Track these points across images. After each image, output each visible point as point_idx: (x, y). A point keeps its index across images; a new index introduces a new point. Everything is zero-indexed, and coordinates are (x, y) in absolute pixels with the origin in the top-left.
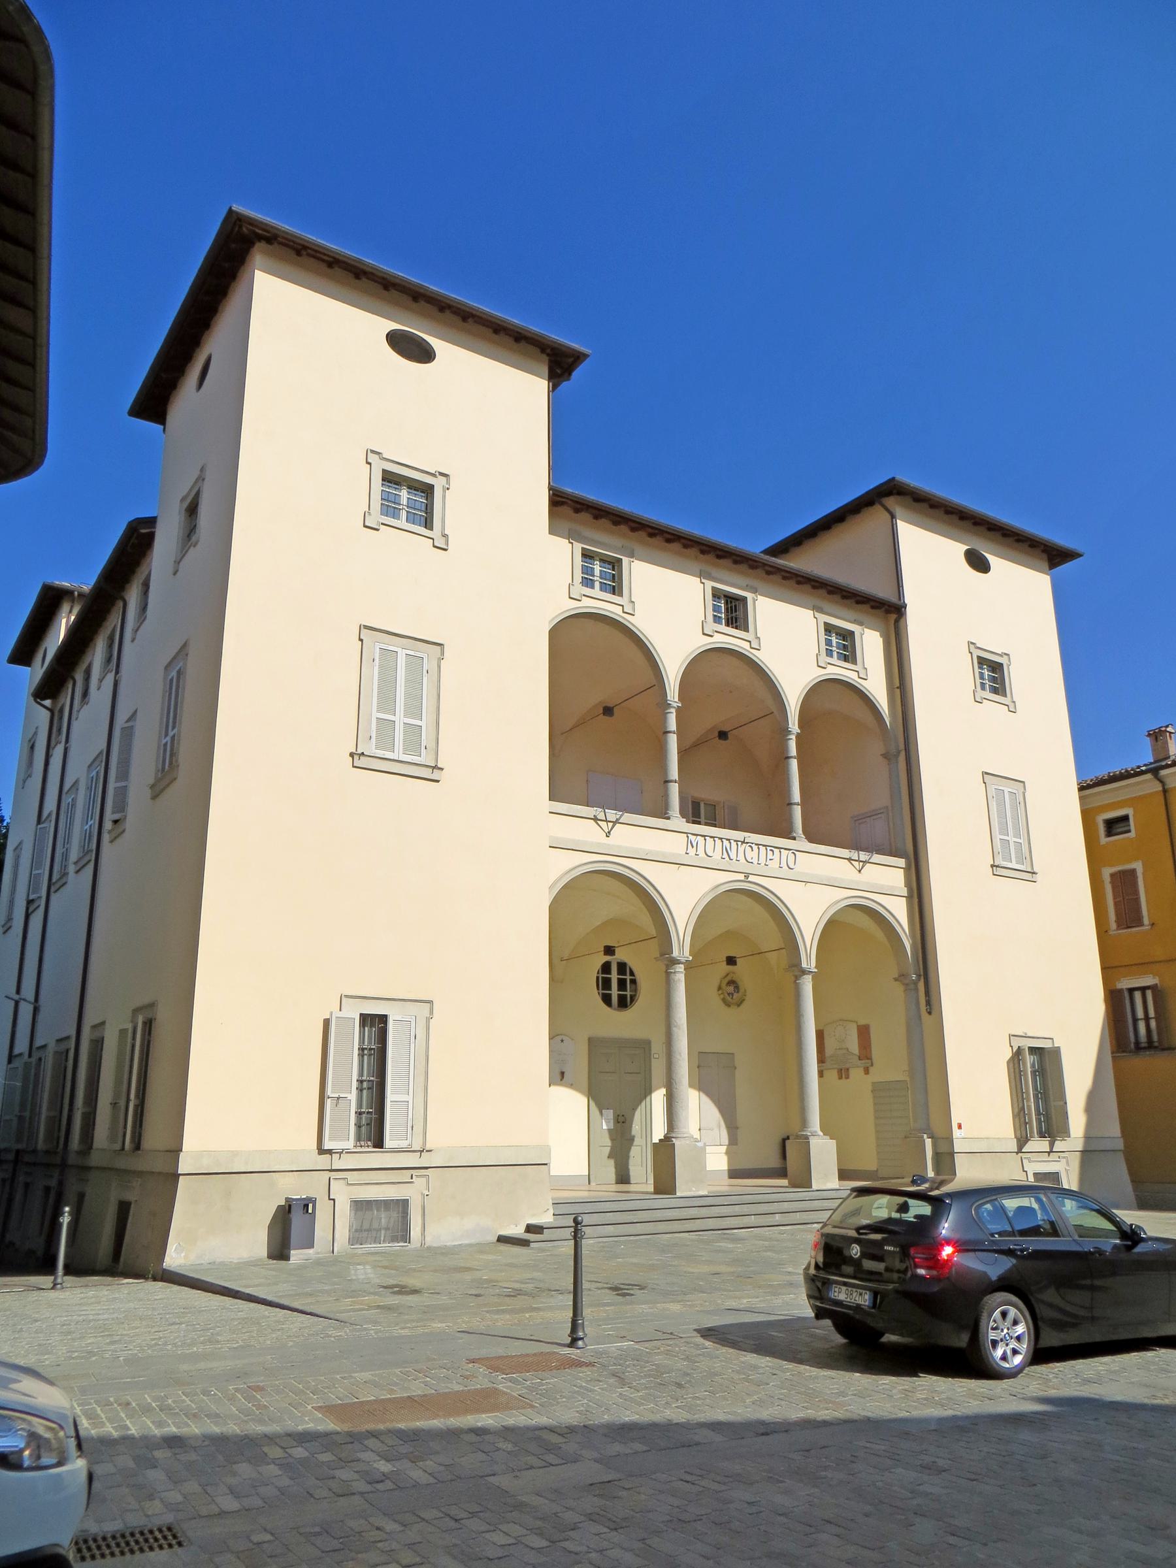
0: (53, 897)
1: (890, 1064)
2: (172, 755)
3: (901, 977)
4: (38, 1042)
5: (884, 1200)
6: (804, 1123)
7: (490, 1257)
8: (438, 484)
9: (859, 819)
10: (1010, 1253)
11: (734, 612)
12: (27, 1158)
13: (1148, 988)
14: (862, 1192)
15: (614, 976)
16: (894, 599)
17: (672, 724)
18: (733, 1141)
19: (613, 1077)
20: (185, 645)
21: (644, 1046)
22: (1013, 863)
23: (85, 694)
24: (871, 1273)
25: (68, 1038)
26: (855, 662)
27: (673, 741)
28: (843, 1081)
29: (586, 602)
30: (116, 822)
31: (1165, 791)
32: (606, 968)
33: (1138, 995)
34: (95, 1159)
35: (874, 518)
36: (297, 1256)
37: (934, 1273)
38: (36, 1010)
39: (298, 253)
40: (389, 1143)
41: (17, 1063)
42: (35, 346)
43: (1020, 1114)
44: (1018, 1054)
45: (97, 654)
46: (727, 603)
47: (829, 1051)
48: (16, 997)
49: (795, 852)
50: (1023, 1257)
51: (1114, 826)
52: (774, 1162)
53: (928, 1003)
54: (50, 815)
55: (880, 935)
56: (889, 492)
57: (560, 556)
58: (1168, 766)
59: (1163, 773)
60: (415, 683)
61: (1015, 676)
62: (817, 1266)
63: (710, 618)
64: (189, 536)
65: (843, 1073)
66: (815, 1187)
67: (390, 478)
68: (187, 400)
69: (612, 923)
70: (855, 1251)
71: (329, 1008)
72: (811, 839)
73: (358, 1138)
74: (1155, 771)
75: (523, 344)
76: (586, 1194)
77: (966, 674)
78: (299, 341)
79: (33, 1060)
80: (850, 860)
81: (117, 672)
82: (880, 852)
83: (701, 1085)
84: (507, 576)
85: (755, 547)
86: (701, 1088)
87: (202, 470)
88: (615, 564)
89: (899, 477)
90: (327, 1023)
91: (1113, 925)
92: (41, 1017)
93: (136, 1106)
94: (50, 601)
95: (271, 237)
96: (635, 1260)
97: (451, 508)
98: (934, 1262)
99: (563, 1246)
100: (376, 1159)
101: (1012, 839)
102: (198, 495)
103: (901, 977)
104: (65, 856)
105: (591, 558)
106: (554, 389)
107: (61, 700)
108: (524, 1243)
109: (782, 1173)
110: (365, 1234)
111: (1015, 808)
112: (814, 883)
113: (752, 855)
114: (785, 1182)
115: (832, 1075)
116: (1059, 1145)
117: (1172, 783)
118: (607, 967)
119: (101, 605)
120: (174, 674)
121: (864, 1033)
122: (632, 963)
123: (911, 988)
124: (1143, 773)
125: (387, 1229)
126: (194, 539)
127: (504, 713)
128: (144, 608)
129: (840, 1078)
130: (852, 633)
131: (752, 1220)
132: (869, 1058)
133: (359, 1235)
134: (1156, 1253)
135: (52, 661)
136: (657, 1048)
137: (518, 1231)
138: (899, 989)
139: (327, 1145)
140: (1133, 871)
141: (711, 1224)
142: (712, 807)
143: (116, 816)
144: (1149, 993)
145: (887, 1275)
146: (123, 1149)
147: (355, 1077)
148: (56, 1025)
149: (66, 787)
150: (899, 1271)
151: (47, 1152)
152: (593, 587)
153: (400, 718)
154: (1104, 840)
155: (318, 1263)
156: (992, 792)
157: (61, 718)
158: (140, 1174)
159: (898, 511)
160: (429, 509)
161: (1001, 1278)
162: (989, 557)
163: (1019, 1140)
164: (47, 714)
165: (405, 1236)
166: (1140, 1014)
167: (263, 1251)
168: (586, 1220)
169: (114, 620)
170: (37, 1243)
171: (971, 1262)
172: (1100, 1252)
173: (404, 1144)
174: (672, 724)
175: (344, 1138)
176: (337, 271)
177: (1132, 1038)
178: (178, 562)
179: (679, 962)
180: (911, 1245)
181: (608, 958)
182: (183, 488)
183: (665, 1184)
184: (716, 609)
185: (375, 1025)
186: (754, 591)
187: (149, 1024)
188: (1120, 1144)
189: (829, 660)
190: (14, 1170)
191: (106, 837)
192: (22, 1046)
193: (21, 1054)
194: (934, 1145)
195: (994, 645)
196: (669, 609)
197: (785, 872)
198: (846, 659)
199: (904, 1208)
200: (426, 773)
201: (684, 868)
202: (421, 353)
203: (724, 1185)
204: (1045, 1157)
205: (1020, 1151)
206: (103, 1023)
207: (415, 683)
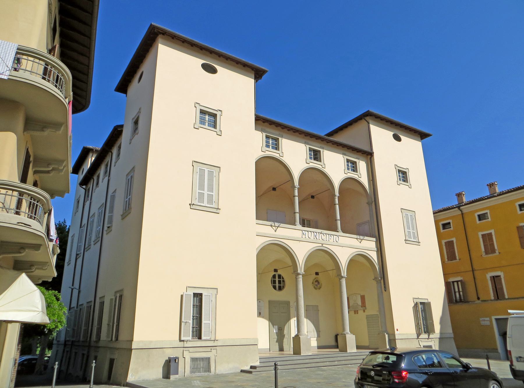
0: (85, 253)
1: (372, 309)
2: (129, 204)
3: (375, 279)
4: (80, 303)
5: (380, 356)
6: (344, 329)
7: (239, 377)
8: (218, 114)
9: (359, 225)
10: (426, 373)
11: (316, 156)
12: (76, 344)
13: (459, 281)
14: (373, 353)
15: (277, 279)
16: (370, 151)
17: (296, 193)
18: (319, 336)
19: (277, 313)
20: (134, 168)
21: (288, 303)
22: (412, 239)
23: (97, 184)
24: (378, 381)
25: (91, 302)
26: (357, 172)
27: (297, 199)
28: (356, 314)
29: (267, 153)
30: (108, 227)
31: (462, 214)
32: (274, 276)
33: (456, 284)
34: (101, 344)
35: (362, 124)
36: (173, 377)
37: (401, 381)
38: (79, 292)
39: (173, 38)
40: (203, 337)
41: (72, 310)
42: (88, 69)
43: (417, 325)
44: (416, 305)
45: (102, 170)
46: (314, 153)
47: (351, 304)
48: (73, 287)
49: (338, 236)
50: (431, 375)
51: (445, 226)
52: (333, 343)
53: (385, 287)
54: (85, 225)
55: (368, 264)
56: (367, 115)
57: (258, 138)
58: (463, 205)
59: (461, 208)
60: (211, 180)
61: (411, 176)
62: (359, 379)
63: (308, 158)
64: (135, 131)
65: (356, 312)
66: (348, 352)
67: (202, 112)
68: (134, 87)
69: (277, 261)
70: (373, 373)
71: (183, 291)
72: (344, 232)
73: (193, 336)
74: (459, 207)
75: (246, 68)
76: (268, 355)
77: (394, 176)
78: (174, 69)
79: (78, 309)
80: (357, 239)
81: (109, 177)
82: (367, 236)
83: (307, 317)
84: (242, 144)
85: (322, 134)
86: (307, 318)
87: (140, 109)
88: (277, 140)
89: (370, 110)
90: (182, 296)
91: (446, 260)
92: (516, 300)
93: (116, 325)
94: (85, 153)
95: (164, 33)
96: (289, 378)
97: (222, 121)
98: (400, 377)
99: (353, 367)
100: (199, 343)
101: (411, 231)
102: (138, 117)
103: (375, 279)
104: (90, 239)
105: (269, 138)
106: (256, 81)
107: (89, 186)
108: (250, 372)
109: (337, 347)
110: (195, 370)
111: (412, 220)
112: (345, 247)
113: (324, 237)
114: (338, 350)
115: (352, 313)
116: (431, 336)
117: (464, 211)
118: (275, 275)
119: (103, 155)
120: (130, 177)
121: (363, 298)
122: (283, 275)
123: (378, 282)
124: (455, 208)
125: (203, 368)
126: (137, 132)
127: (241, 190)
128: (118, 155)
129: (355, 313)
130: (356, 162)
131: (328, 364)
132: (365, 306)
133: (194, 370)
134: (475, 372)
135: (86, 173)
136: (293, 304)
137: (247, 368)
138: (374, 283)
139: (182, 339)
140: (453, 241)
141: (314, 365)
142: (309, 221)
143: (109, 225)
144: (459, 283)
145: (383, 382)
146: (112, 340)
147: (192, 315)
148: (86, 298)
149: (91, 215)
150: (387, 380)
151: (82, 341)
152: (269, 148)
153: (206, 192)
154: (442, 231)
155: (180, 380)
156: (404, 215)
157: (89, 192)
158: (118, 349)
159: (370, 121)
160: (215, 122)
161: (423, 382)
162: (401, 136)
163: (417, 334)
164: (84, 190)
165: (209, 370)
166: (457, 290)
167: (161, 376)
168: (279, 363)
169: (108, 159)
170: (80, 374)
171: (413, 377)
172: (456, 372)
173: (208, 338)
174: (296, 193)
175: (188, 336)
176: (186, 44)
177: (454, 299)
178: (131, 140)
179: (300, 274)
180: (392, 371)
181: (275, 273)
182: (133, 115)
183: (297, 351)
184: (310, 154)
185: (198, 297)
186: (323, 148)
187: (121, 296)
188: (452, 336)
189: (348, 171)
190: (71, 348)
191: (105, 232)
192: (74, 304)
193: (74, 307)
194: (389, 337)
195: (403, 166)
196: (295, 155)
197: (335, 243)
198: (354, 171)
199: (387, 358)
200: (215, 210)
201: (301, 242)
202: (213, 71)
203: (316, 351)
204: (427, 340)
205: (418, 338)
206: (104, 296)
207: (211, 180)
